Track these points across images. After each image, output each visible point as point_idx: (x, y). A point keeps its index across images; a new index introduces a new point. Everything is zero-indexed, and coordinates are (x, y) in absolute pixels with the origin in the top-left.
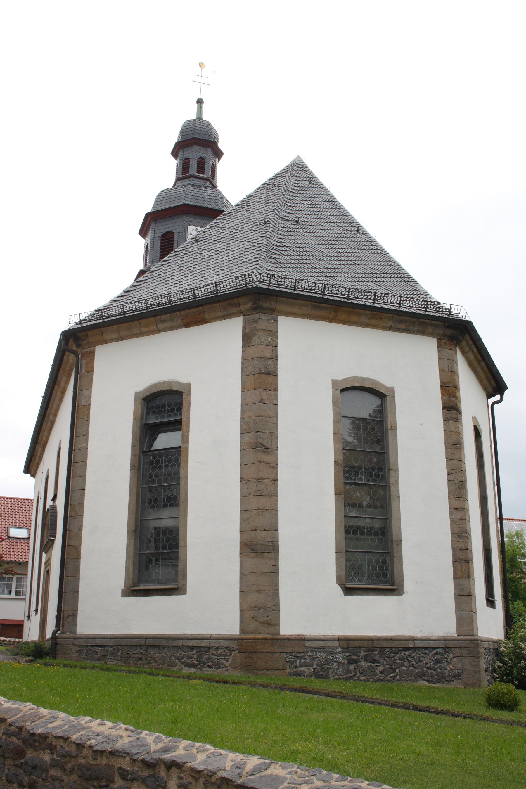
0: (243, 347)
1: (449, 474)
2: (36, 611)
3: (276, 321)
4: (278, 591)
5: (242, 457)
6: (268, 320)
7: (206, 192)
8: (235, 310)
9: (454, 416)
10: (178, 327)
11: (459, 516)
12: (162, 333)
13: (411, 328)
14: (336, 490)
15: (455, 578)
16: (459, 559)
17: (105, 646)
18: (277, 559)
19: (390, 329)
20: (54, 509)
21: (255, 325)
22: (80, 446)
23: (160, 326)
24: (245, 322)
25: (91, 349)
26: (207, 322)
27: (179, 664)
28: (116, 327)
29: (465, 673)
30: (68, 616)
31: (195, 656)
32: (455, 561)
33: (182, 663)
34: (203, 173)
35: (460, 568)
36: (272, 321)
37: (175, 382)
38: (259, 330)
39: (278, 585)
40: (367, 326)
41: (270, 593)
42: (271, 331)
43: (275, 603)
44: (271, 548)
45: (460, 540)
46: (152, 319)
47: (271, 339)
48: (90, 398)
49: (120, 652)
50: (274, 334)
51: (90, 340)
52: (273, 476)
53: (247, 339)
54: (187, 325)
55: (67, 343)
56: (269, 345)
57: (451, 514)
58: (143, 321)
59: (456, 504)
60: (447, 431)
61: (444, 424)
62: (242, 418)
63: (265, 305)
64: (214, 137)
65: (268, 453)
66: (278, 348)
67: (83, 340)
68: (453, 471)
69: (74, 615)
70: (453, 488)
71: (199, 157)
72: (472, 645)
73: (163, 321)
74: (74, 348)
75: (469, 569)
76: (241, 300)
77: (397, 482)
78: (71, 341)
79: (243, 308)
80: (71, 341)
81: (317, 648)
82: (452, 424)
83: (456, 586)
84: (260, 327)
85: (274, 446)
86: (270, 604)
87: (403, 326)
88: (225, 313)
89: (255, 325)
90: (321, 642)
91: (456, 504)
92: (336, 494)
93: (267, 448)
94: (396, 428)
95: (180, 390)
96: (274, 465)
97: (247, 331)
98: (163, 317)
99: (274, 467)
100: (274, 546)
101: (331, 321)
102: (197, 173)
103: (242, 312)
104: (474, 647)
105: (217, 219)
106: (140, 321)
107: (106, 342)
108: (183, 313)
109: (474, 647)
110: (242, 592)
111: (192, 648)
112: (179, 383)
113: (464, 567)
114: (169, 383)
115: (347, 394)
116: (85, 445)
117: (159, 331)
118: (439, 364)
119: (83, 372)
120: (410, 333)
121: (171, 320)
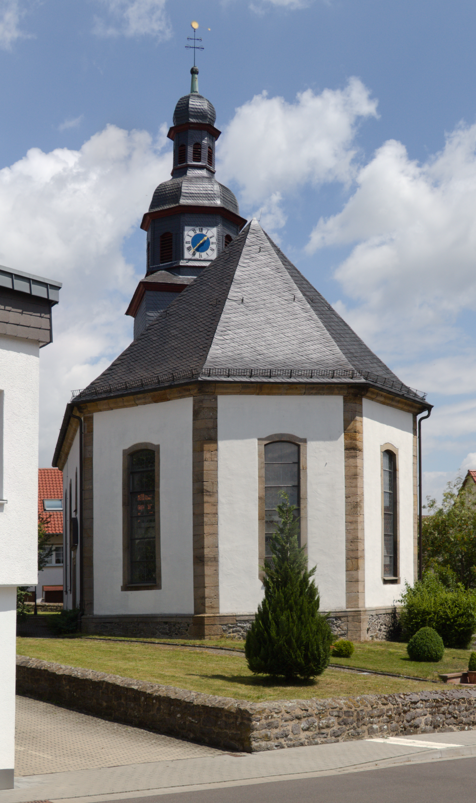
0: (194, 420)
1: (346, 497)
2: (70, 590)
3: (216, 399)
4: (218, 586)
5: (194, 499)
6: (210, 400)
7: (201, 186)
8: (188, 393)
9: (354, 454)
10: (150, 403)
11: (352, 527)
12: (139, 406)
13: (321, 392)
14: (259, 517)
15: (347, 571)
16: (351, 557)
17: (112, 623)
18: (217, 566)
19: (304, 394)
20: (76, 519)
21: (201, 404)
22: (88, 487)
23: (137, 402)
24: (194, 401)
25: (90, 415)
26: (169, 400)
27: (158, 632)
28: (106, 401)
29: (349, 632)
30: (88, 604)
31: (167, 628)
32: (347, 559)
33: (160, 632)
34: (199, 160)
35: (351, 563)
36: (214, 400)
37: (149, 443)
38: (204, 408)
39: (218, 582)
40: (286, 394)
41: (213, 588)
42: (212, 408)
43: (216, 594)
44: (213, 559)
45: (352, 544)
46: (131, 397)
47: (213, 414)
48: (92, 452)
49: (122, 627)
50: (215, 409)
51: (89, 409)
52: (214, 511)
53: (196, 414)
54: (156, 402)
55: (72, 411)
56: (211, 418)
57: (346, 526)
58: (125, 398)
59: (351, 519)
60: (347, 467)
61: (345, 462)
62: (194, 472)
63: (207, 390)
64: (209, 116)
65: (210, 495)
66: (218, 419)
67: (84, 409)
68: (351, 495)
69: (91, 604)
70: (349, 508)
71: (194, 143)
72: (356, 614)
73: (139, 399)
74: (78, 414)
75: (358, 564)
76: (190, 387)
77: (306, 507)
78: (75, 408)
79: (192, 392)
80: (75, 408)
81: (243, 621)
82: (351, 460)
83: (347, 576)
84: (204, 406)
85: (215, 490)
86: (213, 595)
87: (314, 392)
88: (180, 395)
89: (201, 404)
90: (247, 617)
91: (351, 519)
92: (259, 520)
93: (210, 492)
94: (306, 468)
95: (153, 449)
96: (215, 504)
97: (196, 408)
98: (139, 396)
99: (215, 505)
100: (215, 558)
101: (258, 394)
102: (194, 161)
103: (192, 395)
104: (357, 616)
105: (184, 290)
106: (123, 398)
107: (100, 411)
108: (152, 393)
109: (357, 616)
110: (195, 587)
111: (166, 623)
112: (152, 444)
113: (354, 563)
114: (146, 444)
115: (270, 446)
116: (91, 486)
117: (137, 405)
118: (344, 416)
119: (86, 432)
120: (321, 395)
121: (144, 398)
